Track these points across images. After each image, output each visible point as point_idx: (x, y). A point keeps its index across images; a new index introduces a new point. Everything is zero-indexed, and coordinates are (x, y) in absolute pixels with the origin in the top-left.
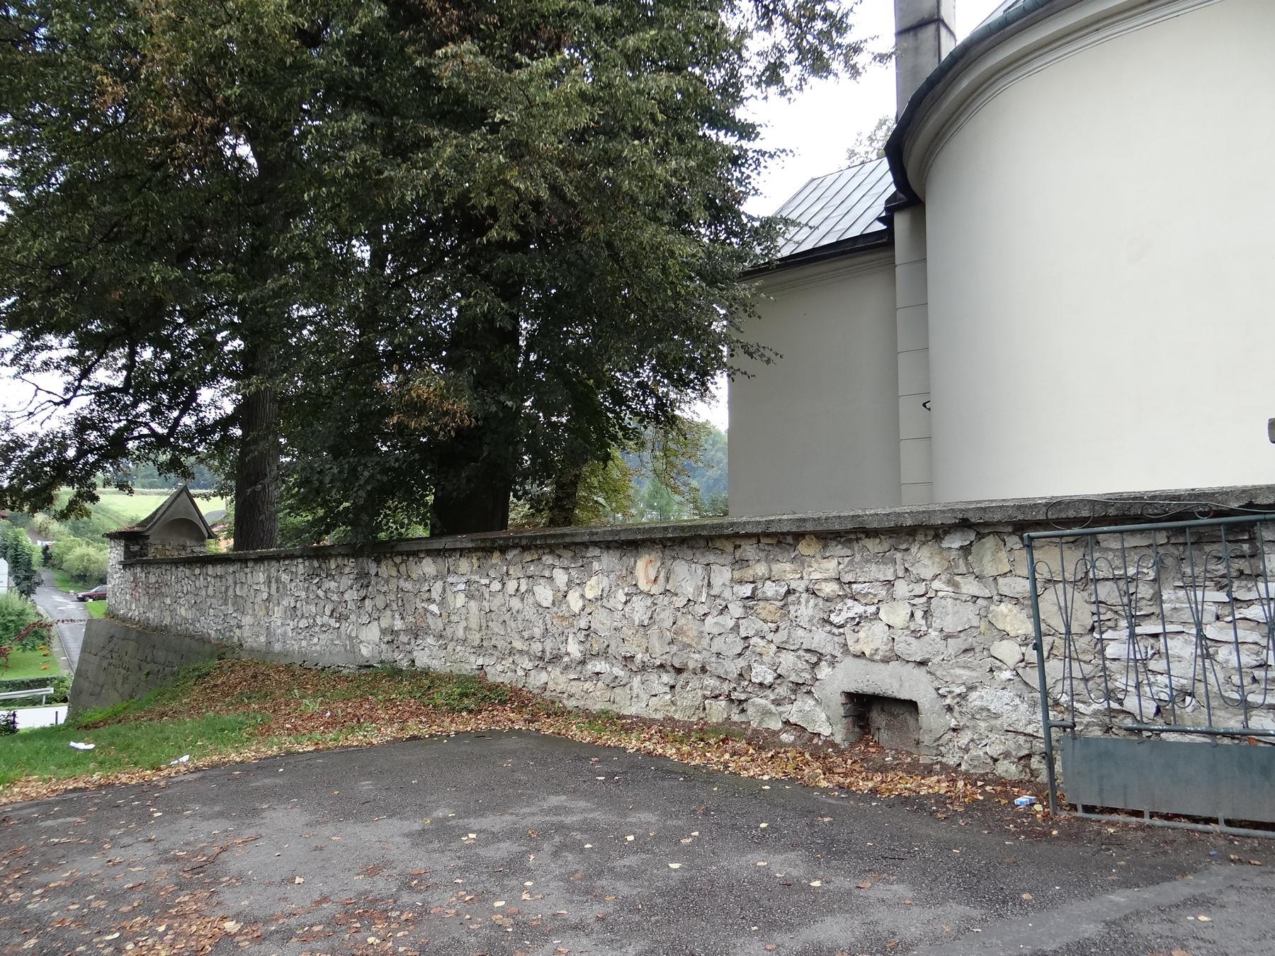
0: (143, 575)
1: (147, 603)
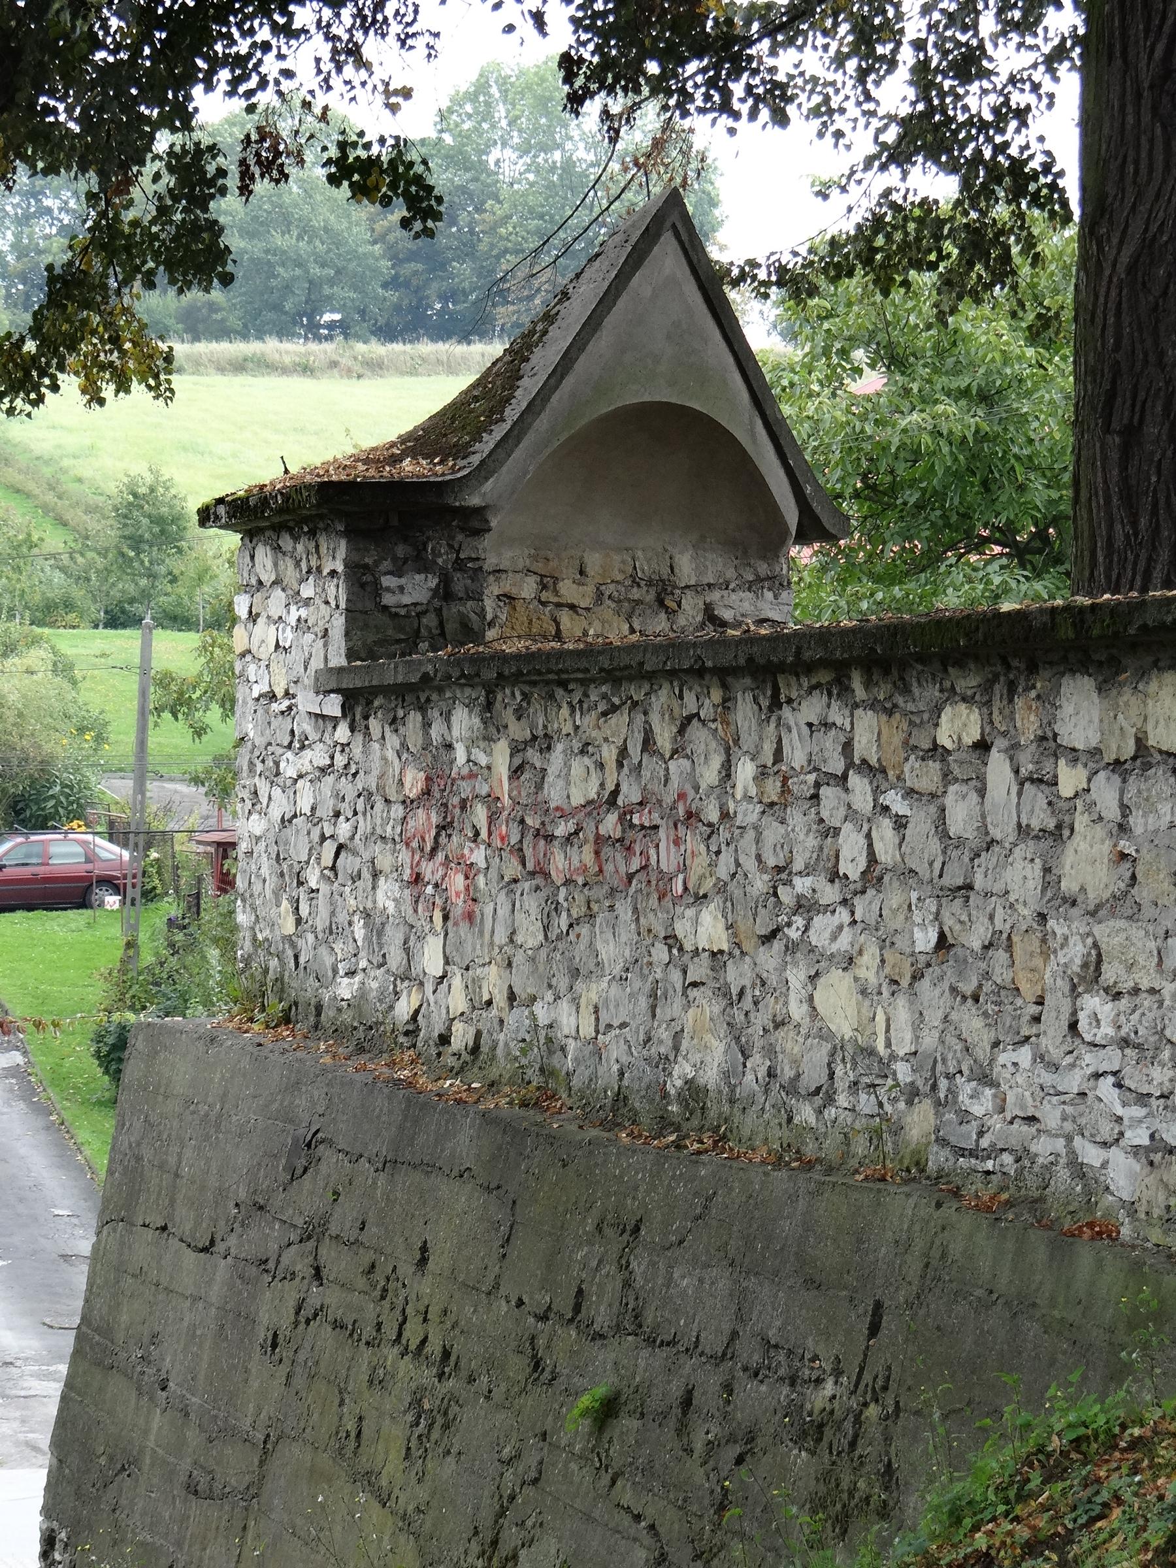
0: (501, 758)
1: (531, 935)
